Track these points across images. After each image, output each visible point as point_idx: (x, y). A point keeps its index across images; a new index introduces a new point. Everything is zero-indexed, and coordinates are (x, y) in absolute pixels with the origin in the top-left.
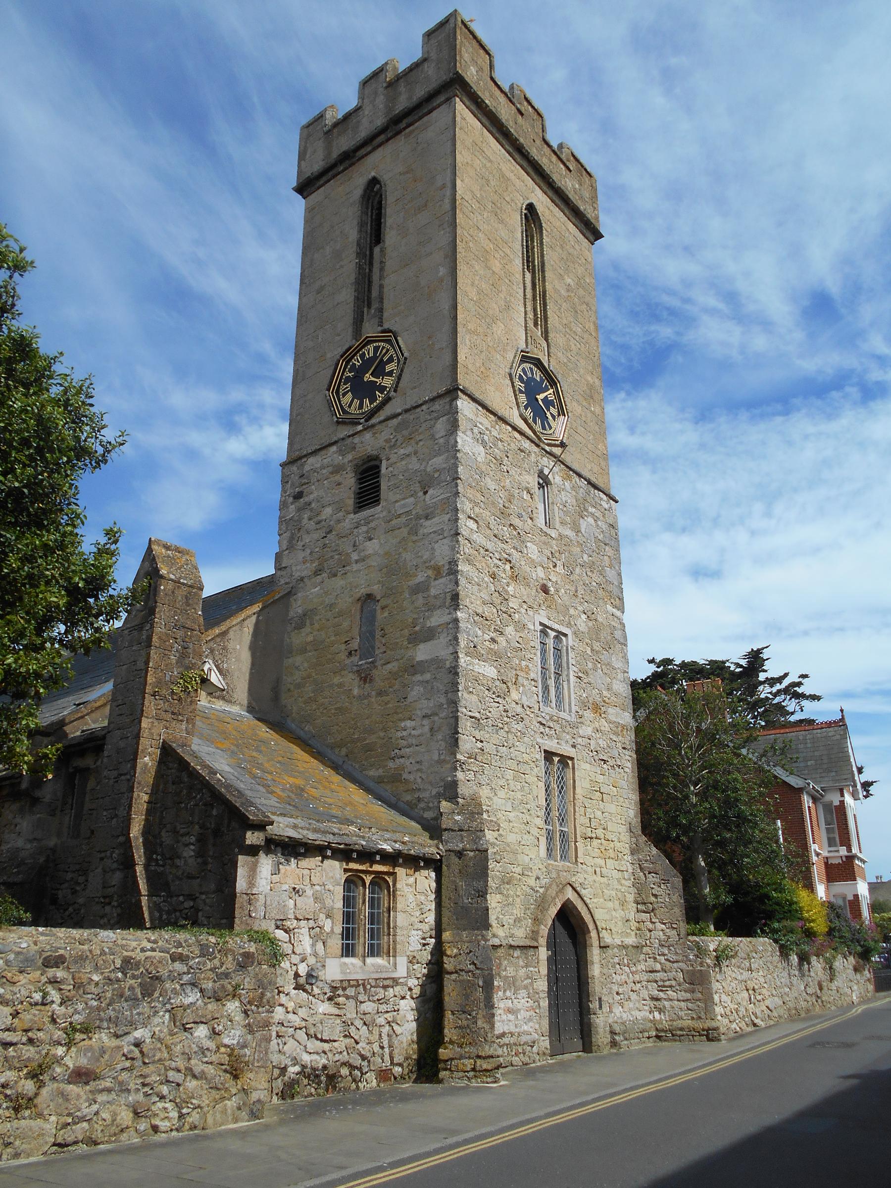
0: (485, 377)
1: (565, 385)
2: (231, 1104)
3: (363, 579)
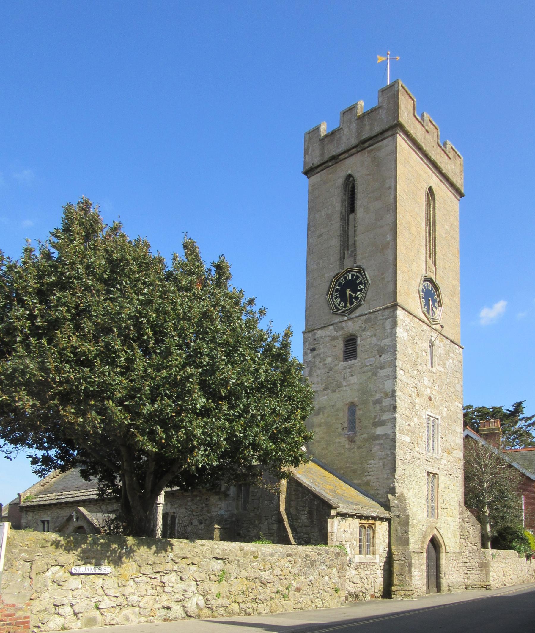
2: (336, 600)
3: (348, 395)
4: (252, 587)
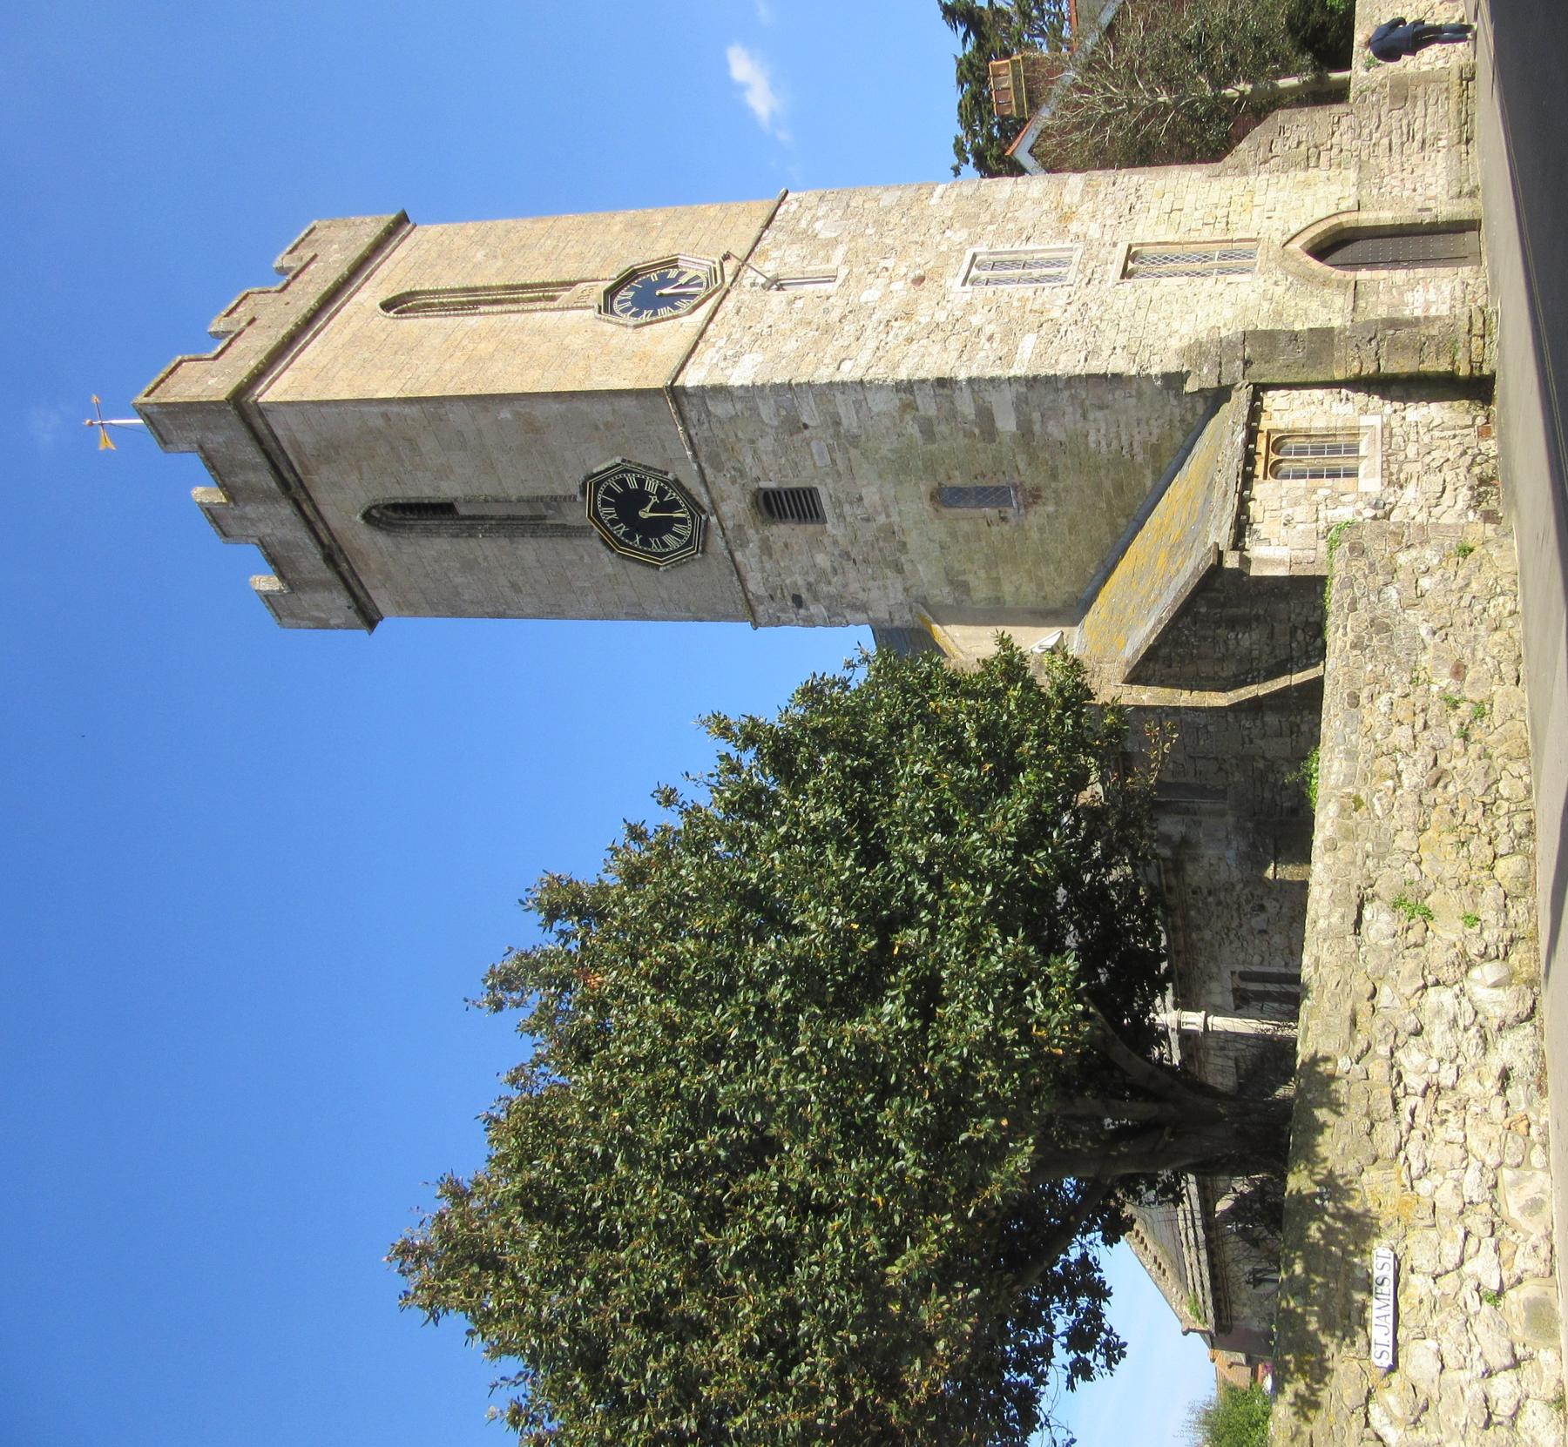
0: (645, 357)
1: (636, 260)
2: (1495, 553)
3: (911, 507)
4: (1448, 816)
